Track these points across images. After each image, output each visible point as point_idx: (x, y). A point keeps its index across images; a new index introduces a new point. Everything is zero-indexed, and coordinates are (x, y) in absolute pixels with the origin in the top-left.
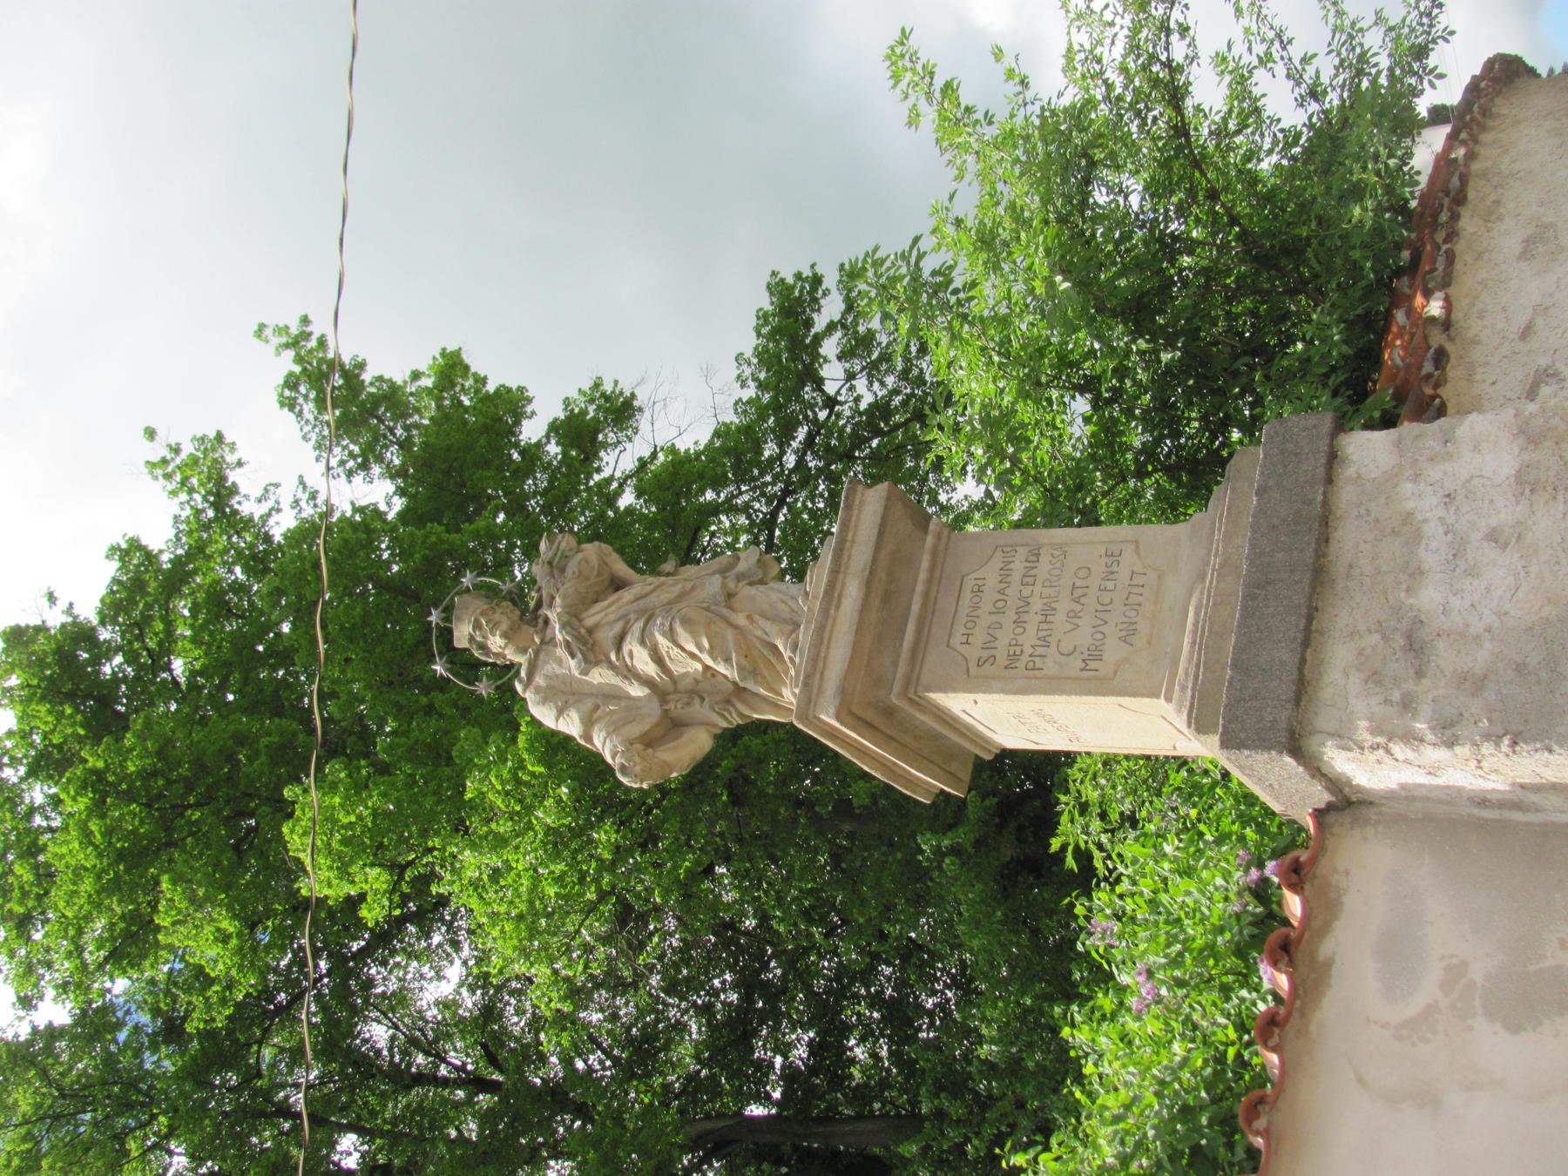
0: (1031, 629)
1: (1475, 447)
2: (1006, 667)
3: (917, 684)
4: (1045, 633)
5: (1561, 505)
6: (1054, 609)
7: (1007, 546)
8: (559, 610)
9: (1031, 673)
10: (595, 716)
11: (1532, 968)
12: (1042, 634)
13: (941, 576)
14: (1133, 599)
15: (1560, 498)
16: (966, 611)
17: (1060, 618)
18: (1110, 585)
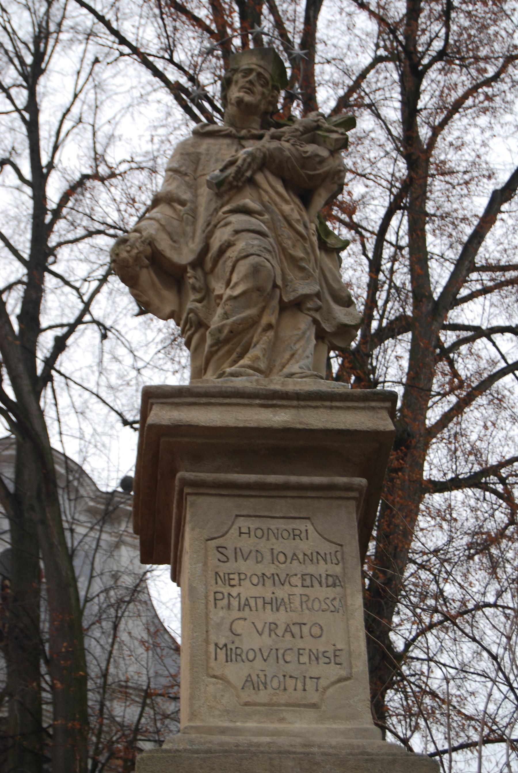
2: (217, 573)
6: (278, 610)
8: (242, 154)
9: (211, 598)
14: (290, 683)
16: (273, 527)
17: (270, 616)
18: (304, 659)
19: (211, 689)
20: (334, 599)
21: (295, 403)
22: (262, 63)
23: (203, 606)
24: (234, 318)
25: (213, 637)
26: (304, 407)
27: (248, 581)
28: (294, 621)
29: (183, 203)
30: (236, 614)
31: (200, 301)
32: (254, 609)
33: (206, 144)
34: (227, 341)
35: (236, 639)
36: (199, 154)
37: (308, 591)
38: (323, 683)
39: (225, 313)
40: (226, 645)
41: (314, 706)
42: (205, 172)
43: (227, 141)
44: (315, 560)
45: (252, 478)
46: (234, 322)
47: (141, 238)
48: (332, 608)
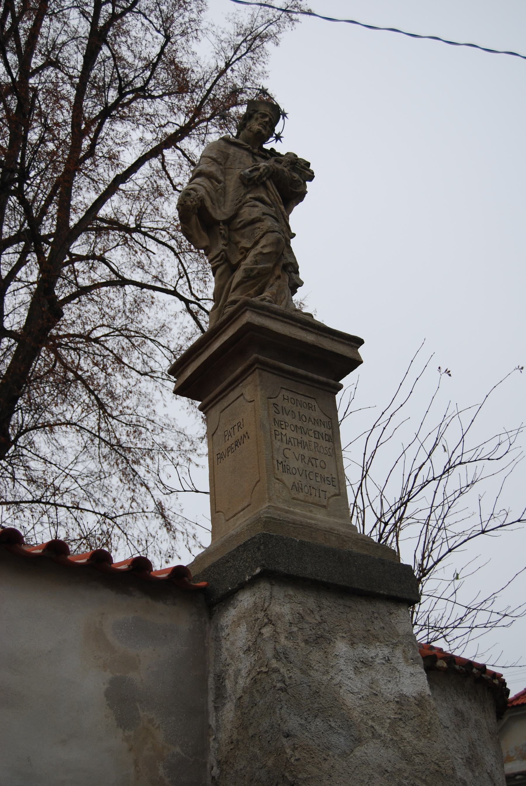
0: (293, 434)
1: (412, 674)
2: (274, 419)
3: (261, 369)
4: (293, 442)
5: (393, 717)
6: (304, 448)
7: (332, 423)
9: (273, 433)
10: (214, 181)
11: (138, 704)
12: (292, 440)
13: (314, 387)
14: (313, 491)
15: (396, 716)
16: (299, 399)
18: (318, 479)
19: (277, 485)
20: (330, 448)
21: (316, 331)
22: (272, 113)
23: (269, 437)
24: (261, 266)
25: (276, 456)
26: (320, 335)
27: (289, 427)
28: (313, 457)
29: (219, 182)
30: (285, 446)
31: (225, 245)
32: (293, 444)
33: (232, 150)
34: (254, 278)
35: (287, 460)
36: (229, 154)
37: (317, 441)
38: (328, 495)
39: (256, 261)
40: (282, 462)
41: (324, 507)
42: (232, 167)
43: (246, 153)
44: (319, 424)
45: (291, 368)
46: (261, 268)
47: (197, 195)
48: (329, 454)
